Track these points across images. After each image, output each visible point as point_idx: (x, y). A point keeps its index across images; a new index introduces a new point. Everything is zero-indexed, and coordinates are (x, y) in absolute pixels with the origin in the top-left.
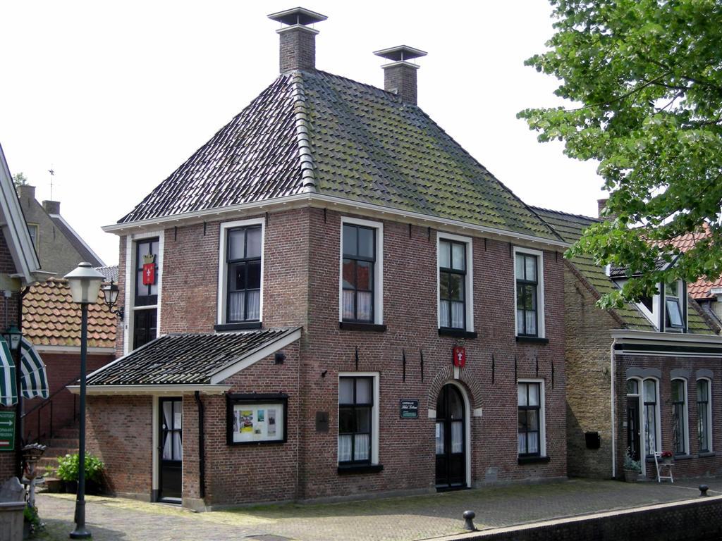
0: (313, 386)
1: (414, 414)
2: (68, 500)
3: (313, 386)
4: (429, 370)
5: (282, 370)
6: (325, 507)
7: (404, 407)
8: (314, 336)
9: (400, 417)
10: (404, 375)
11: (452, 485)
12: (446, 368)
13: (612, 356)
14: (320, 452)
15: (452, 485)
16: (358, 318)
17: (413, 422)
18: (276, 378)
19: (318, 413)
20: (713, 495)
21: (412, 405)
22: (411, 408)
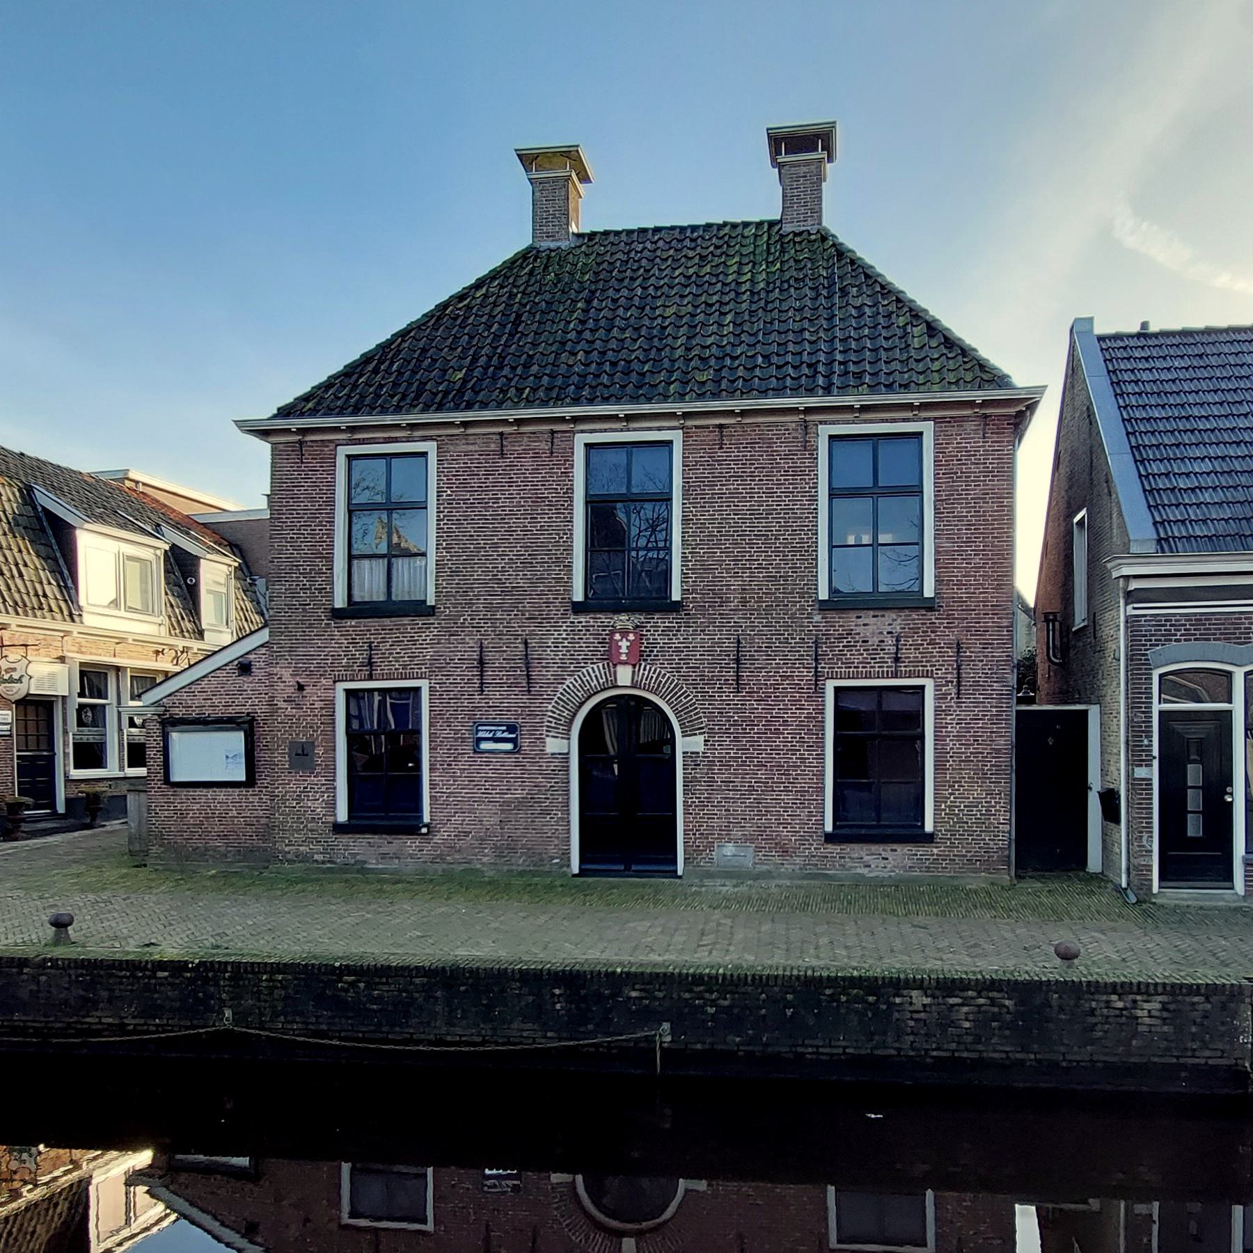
0: (282, 704)
1: (509, 746)
2: (921, 578)
3: (282, 704)
4: (543, 674)
5: (246, 683)
6: (291, 883)
7: (481, 735)
8: (282, 632)
9: (475, 752)
10: (482, 684)
11: (593, 1050)
12: (595, 672)
13: (1122, 618)
14: (299, 799)
15: (593, 1050)
16: (394, 598)
17: (511, 759)
18: (979, 614)
19: (293, 744)
20: (1118, 780)
21: (504, 731)
22: (499, 735)
